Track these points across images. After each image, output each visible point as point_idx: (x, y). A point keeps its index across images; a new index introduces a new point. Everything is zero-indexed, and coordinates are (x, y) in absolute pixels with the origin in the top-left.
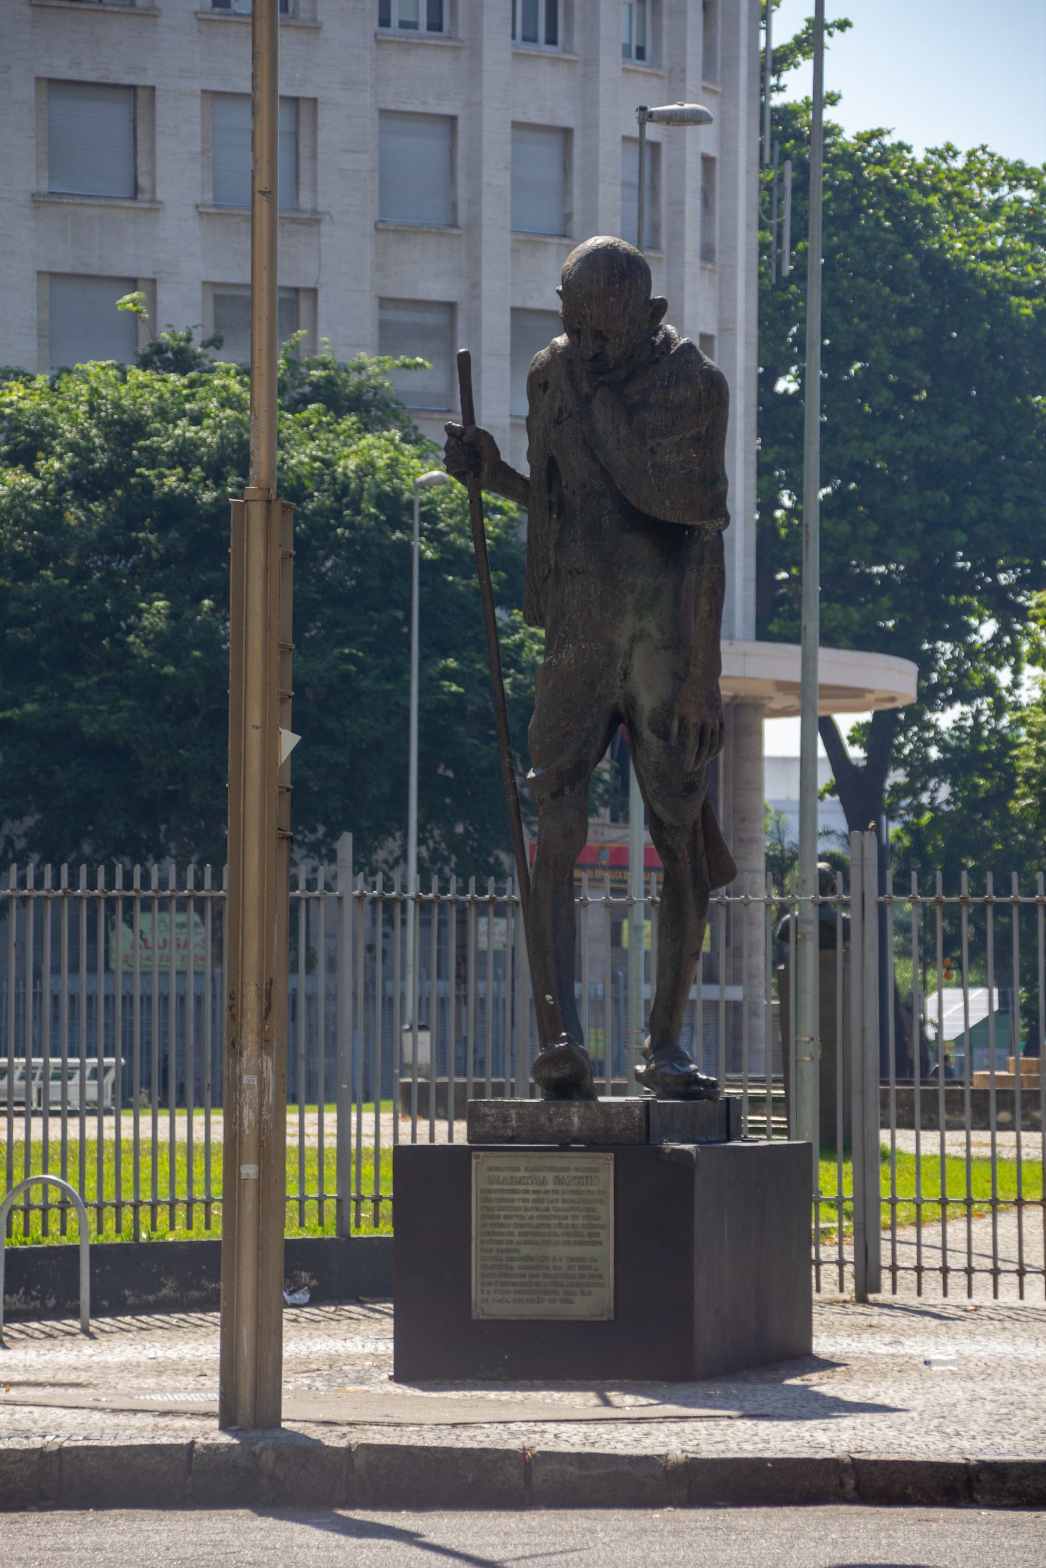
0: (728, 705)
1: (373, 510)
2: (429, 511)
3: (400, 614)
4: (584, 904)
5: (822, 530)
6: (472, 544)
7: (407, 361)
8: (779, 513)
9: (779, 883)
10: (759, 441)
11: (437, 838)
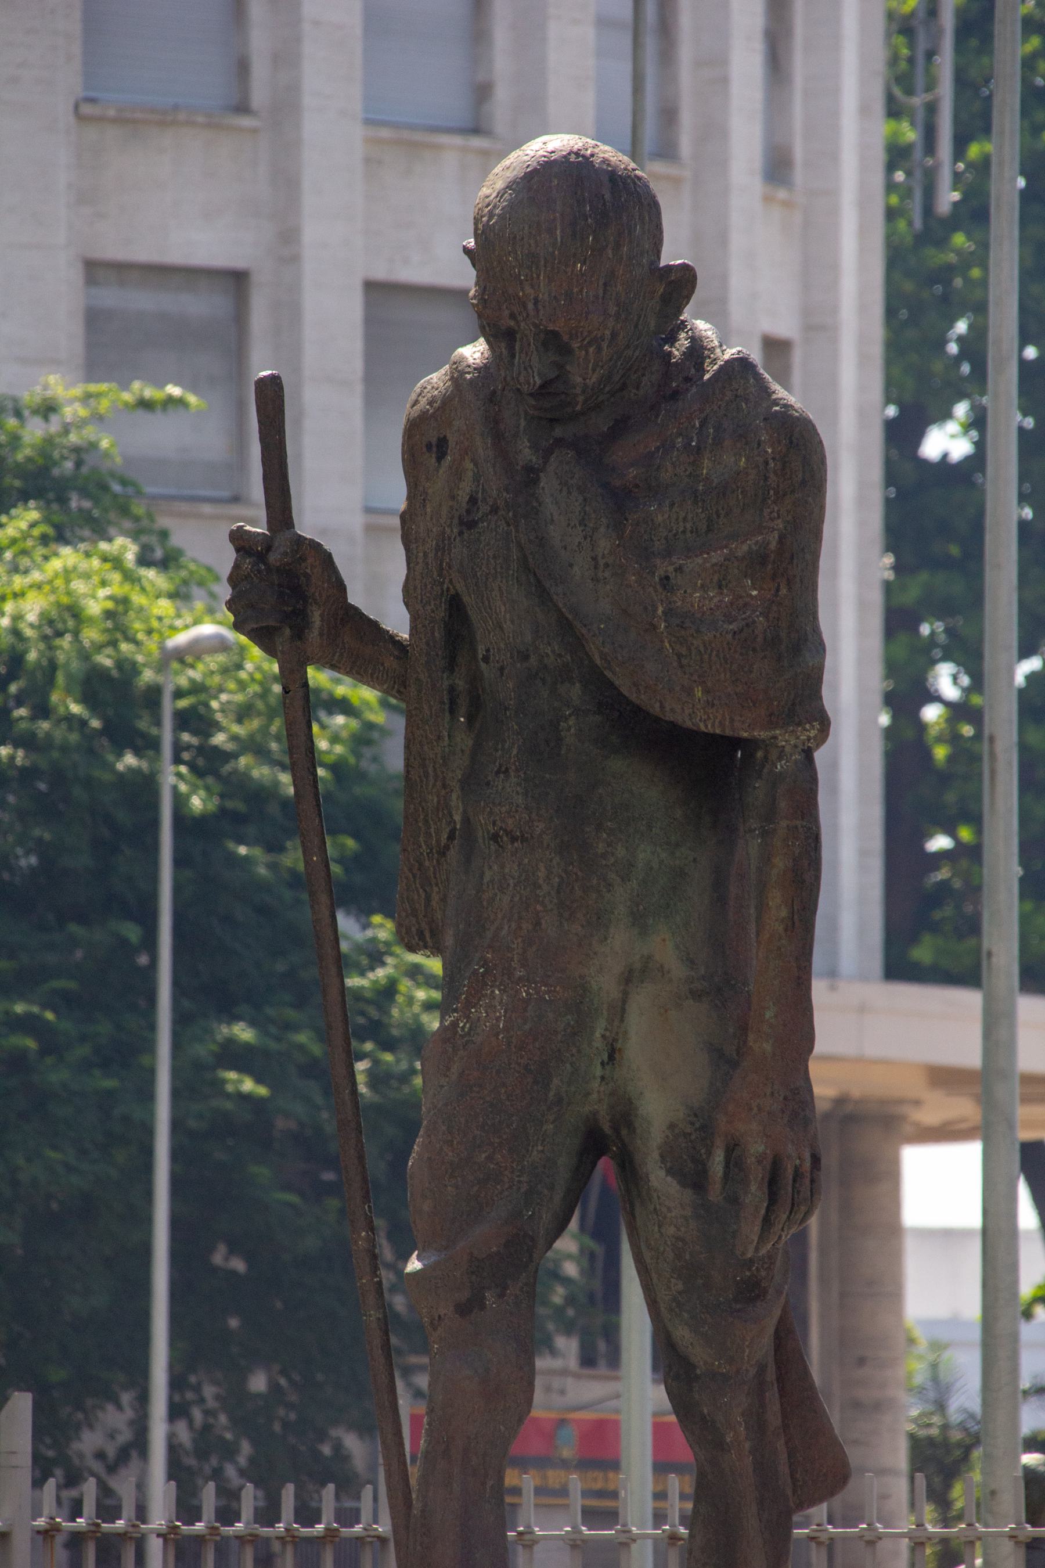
0: (827, 1116)
1: (75, 708)
2: (193, 708)
3: (132, 932)
4: (528, 1541)
5: (1024, 748)
6: (285, 778)
7: (149, 393)
8: (932, 713)
9: (940, 1498)
10: (889, 560)
11: (211, 1403)
